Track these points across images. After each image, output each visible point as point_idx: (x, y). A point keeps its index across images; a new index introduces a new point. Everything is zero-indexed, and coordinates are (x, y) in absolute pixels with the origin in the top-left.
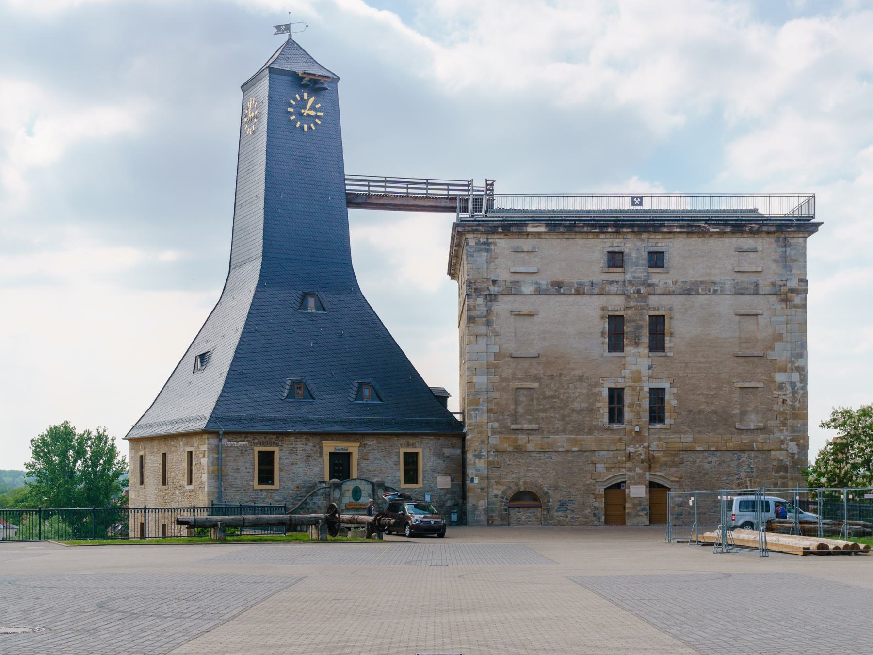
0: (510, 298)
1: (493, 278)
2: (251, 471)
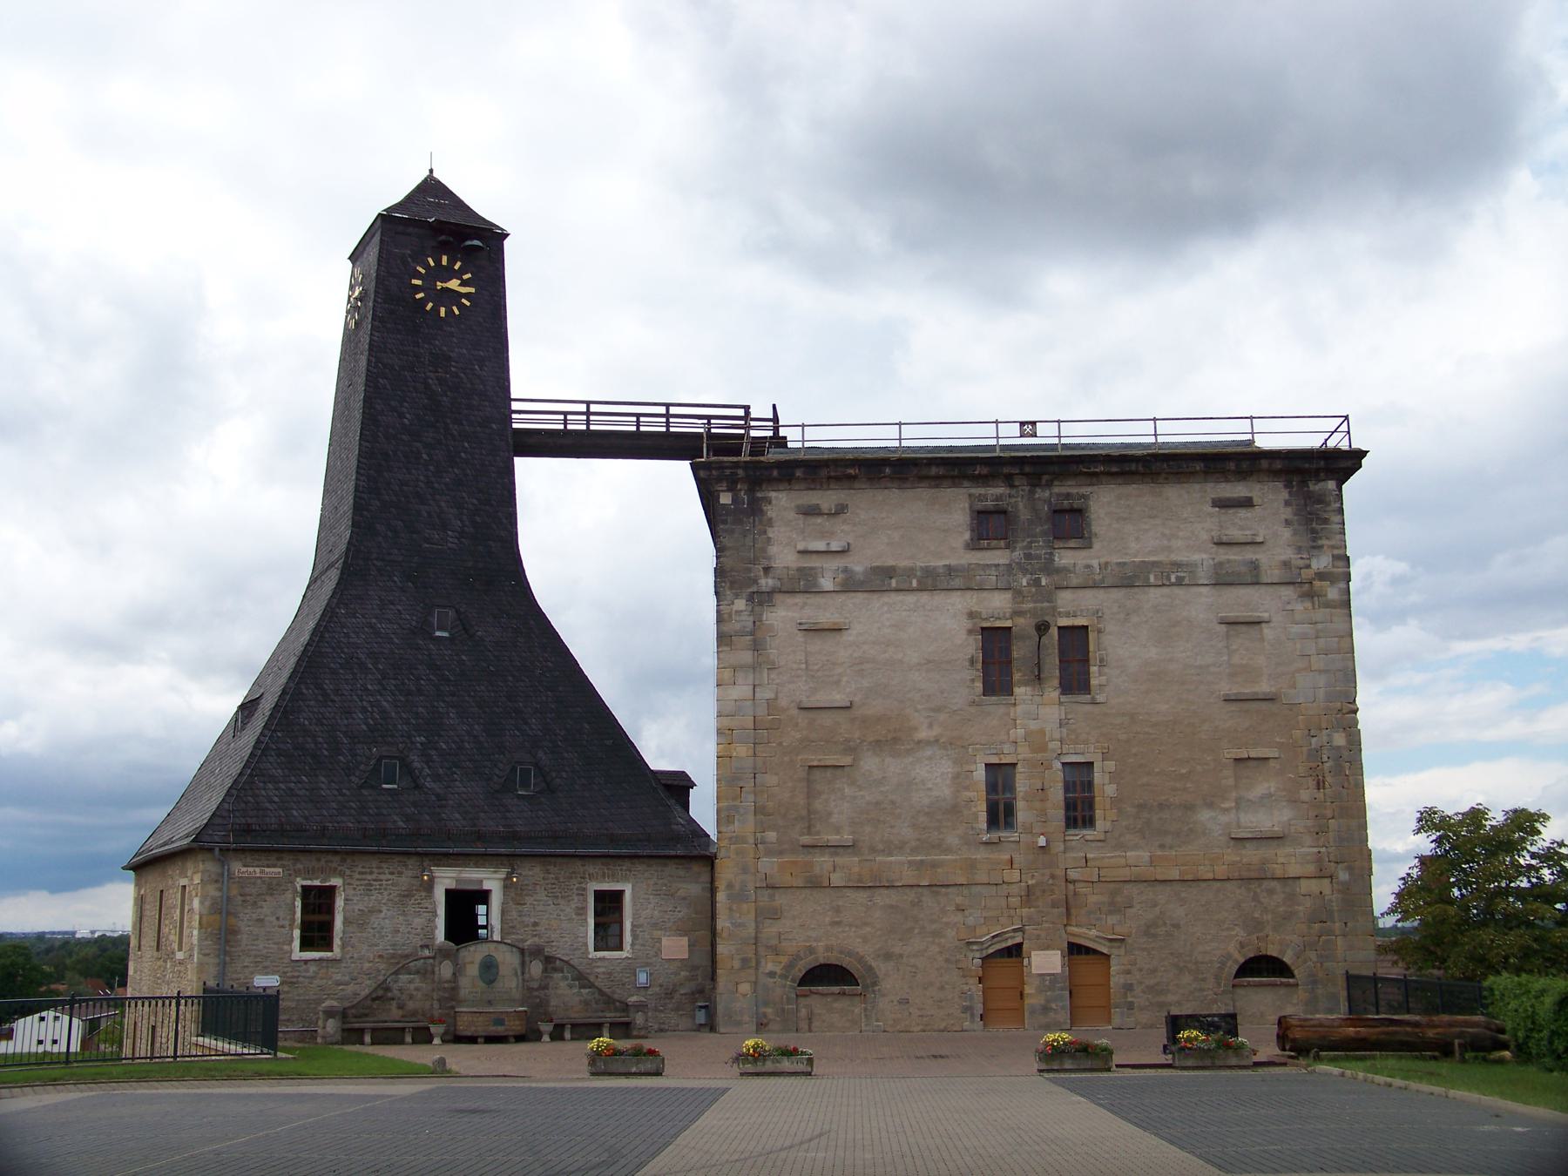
0: (799, 599)
2: (287, 923)
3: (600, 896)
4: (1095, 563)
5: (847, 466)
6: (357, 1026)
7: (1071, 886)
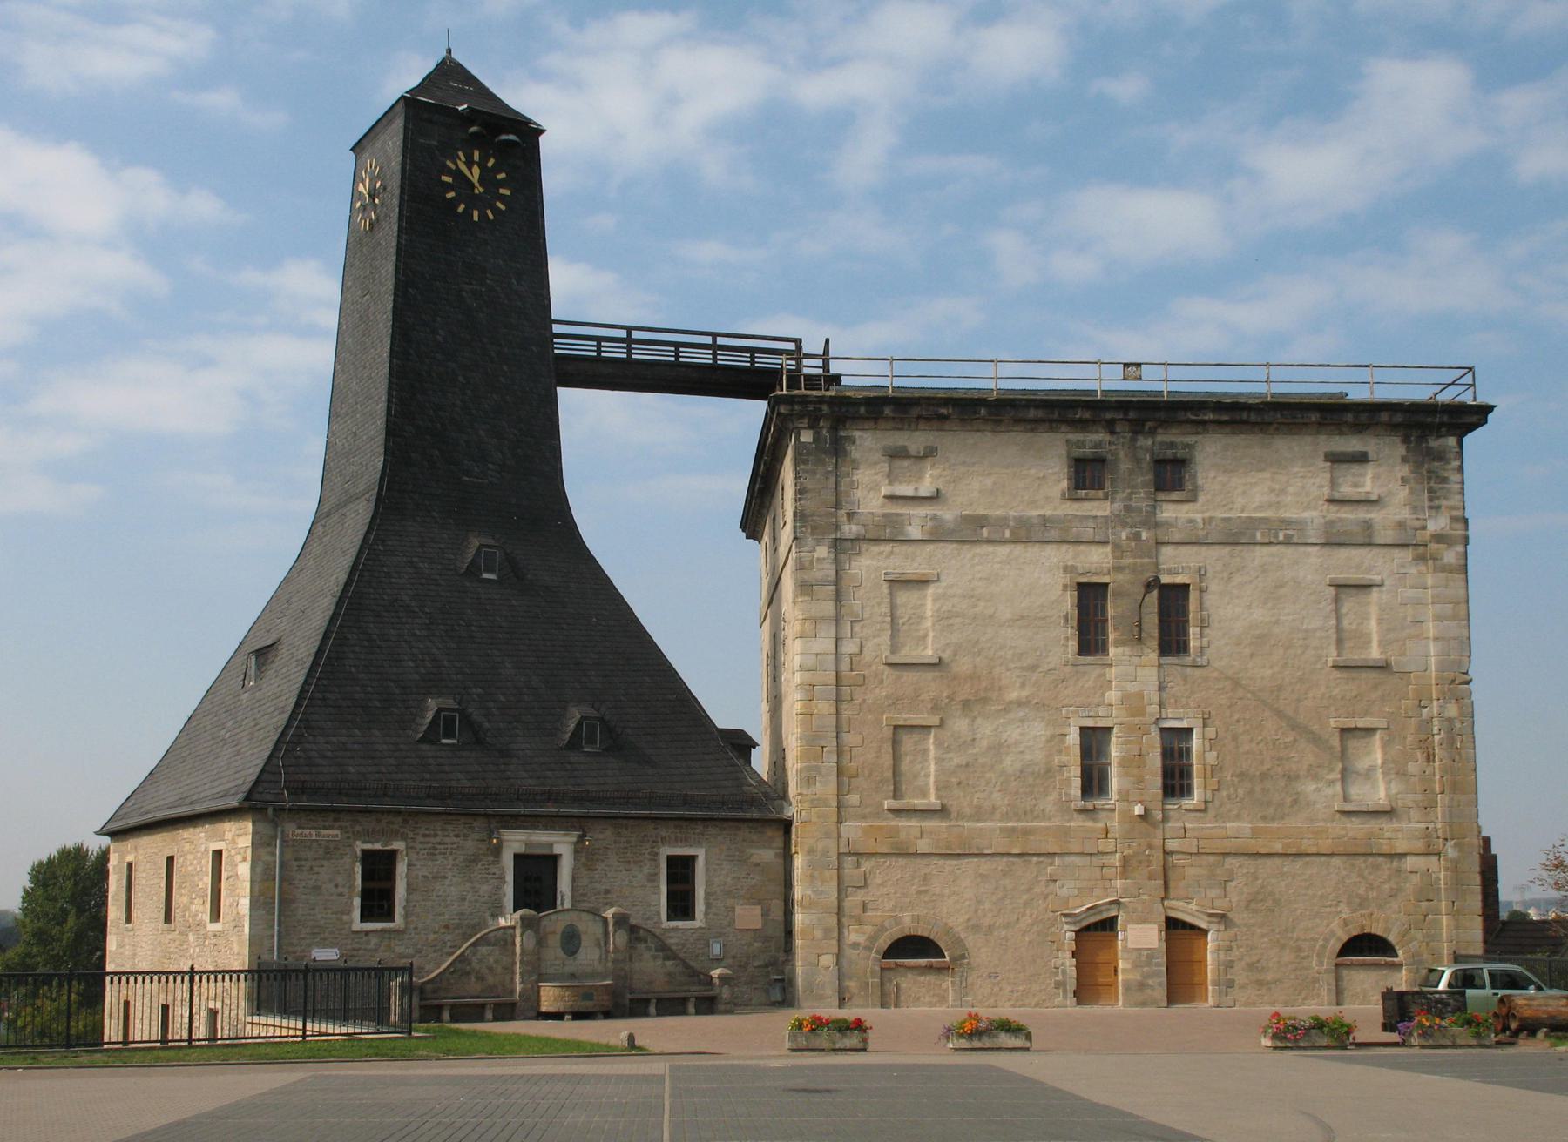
3: (672, 860)
4: (1198, 517)
5: (939, 405)
6: (436, 1002)
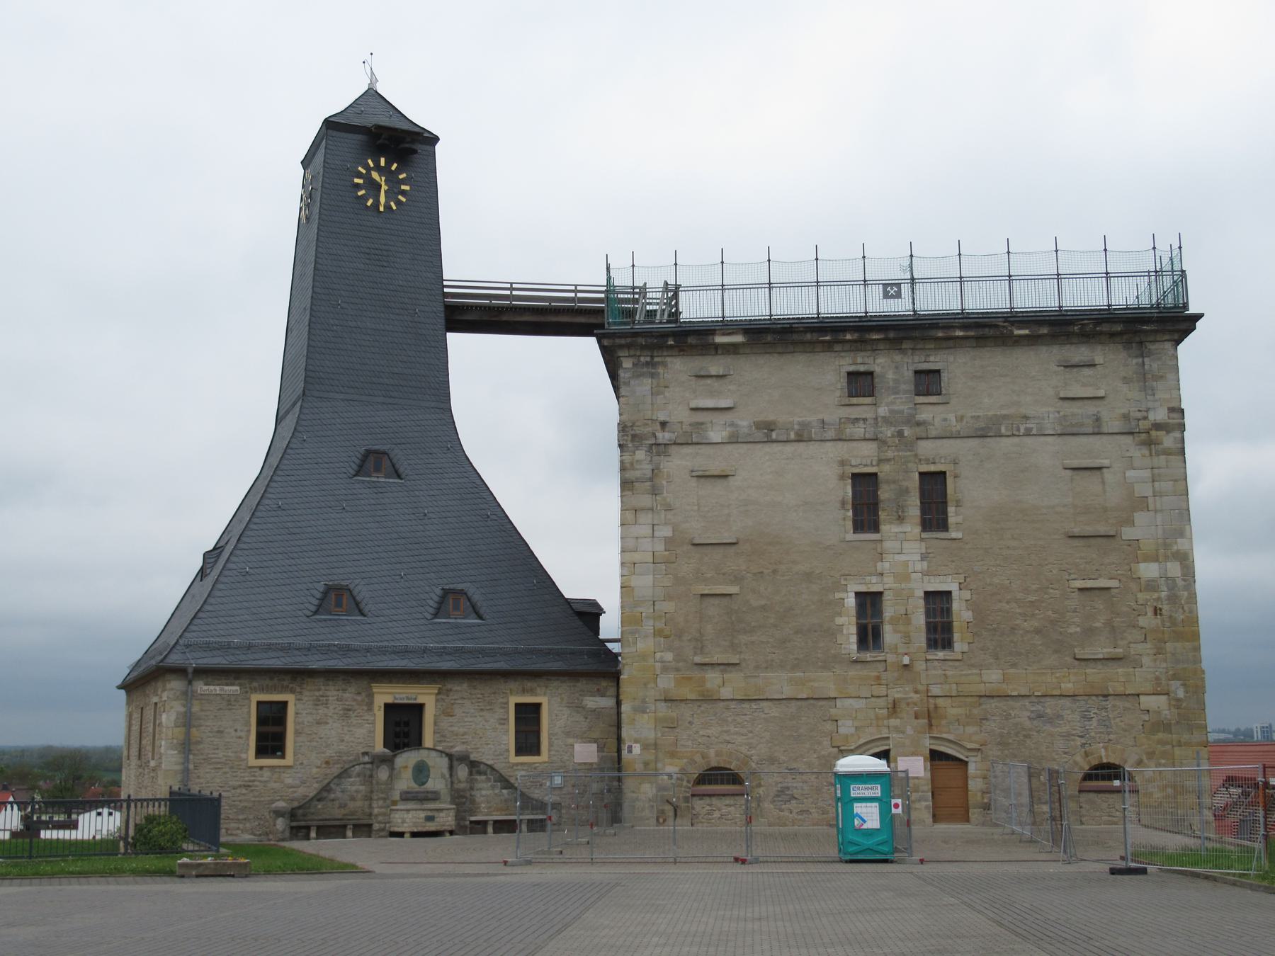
1: (662, 418)
7: (931, 700)
